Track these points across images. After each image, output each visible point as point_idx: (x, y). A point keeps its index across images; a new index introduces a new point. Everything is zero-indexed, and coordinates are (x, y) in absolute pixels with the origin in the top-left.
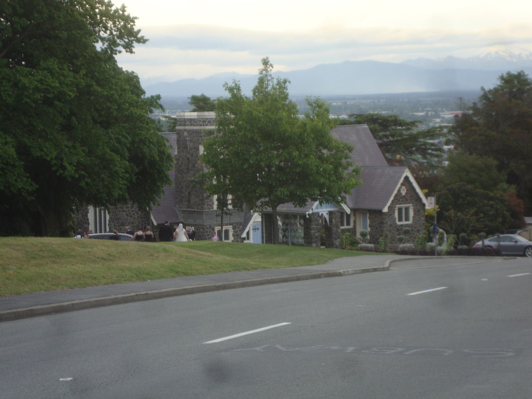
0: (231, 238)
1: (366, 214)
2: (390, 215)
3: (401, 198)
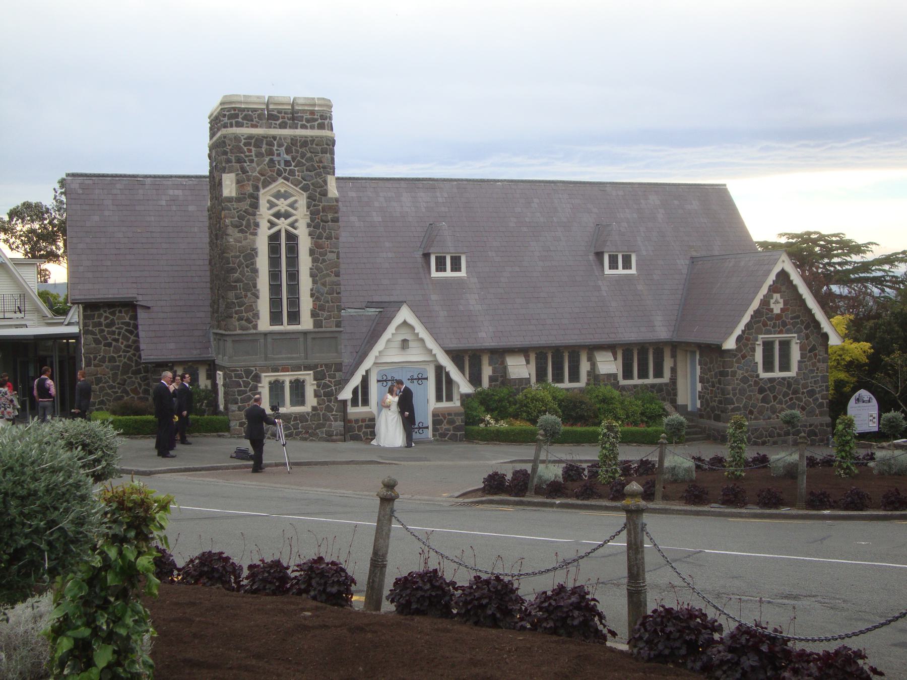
0: (311, 400)
1: (693, 353)
2: (744, 357)
3: (770, 319)
